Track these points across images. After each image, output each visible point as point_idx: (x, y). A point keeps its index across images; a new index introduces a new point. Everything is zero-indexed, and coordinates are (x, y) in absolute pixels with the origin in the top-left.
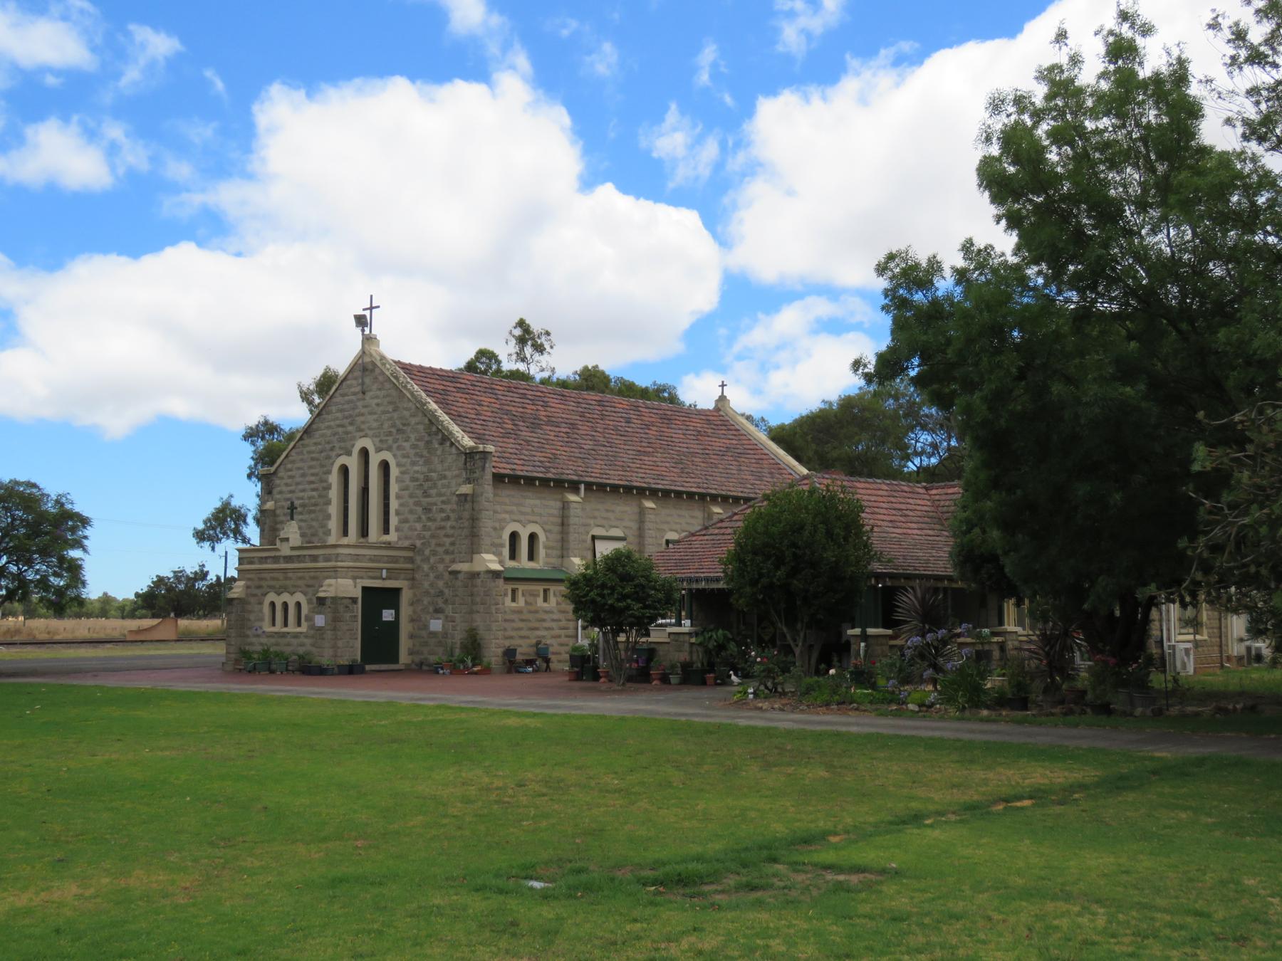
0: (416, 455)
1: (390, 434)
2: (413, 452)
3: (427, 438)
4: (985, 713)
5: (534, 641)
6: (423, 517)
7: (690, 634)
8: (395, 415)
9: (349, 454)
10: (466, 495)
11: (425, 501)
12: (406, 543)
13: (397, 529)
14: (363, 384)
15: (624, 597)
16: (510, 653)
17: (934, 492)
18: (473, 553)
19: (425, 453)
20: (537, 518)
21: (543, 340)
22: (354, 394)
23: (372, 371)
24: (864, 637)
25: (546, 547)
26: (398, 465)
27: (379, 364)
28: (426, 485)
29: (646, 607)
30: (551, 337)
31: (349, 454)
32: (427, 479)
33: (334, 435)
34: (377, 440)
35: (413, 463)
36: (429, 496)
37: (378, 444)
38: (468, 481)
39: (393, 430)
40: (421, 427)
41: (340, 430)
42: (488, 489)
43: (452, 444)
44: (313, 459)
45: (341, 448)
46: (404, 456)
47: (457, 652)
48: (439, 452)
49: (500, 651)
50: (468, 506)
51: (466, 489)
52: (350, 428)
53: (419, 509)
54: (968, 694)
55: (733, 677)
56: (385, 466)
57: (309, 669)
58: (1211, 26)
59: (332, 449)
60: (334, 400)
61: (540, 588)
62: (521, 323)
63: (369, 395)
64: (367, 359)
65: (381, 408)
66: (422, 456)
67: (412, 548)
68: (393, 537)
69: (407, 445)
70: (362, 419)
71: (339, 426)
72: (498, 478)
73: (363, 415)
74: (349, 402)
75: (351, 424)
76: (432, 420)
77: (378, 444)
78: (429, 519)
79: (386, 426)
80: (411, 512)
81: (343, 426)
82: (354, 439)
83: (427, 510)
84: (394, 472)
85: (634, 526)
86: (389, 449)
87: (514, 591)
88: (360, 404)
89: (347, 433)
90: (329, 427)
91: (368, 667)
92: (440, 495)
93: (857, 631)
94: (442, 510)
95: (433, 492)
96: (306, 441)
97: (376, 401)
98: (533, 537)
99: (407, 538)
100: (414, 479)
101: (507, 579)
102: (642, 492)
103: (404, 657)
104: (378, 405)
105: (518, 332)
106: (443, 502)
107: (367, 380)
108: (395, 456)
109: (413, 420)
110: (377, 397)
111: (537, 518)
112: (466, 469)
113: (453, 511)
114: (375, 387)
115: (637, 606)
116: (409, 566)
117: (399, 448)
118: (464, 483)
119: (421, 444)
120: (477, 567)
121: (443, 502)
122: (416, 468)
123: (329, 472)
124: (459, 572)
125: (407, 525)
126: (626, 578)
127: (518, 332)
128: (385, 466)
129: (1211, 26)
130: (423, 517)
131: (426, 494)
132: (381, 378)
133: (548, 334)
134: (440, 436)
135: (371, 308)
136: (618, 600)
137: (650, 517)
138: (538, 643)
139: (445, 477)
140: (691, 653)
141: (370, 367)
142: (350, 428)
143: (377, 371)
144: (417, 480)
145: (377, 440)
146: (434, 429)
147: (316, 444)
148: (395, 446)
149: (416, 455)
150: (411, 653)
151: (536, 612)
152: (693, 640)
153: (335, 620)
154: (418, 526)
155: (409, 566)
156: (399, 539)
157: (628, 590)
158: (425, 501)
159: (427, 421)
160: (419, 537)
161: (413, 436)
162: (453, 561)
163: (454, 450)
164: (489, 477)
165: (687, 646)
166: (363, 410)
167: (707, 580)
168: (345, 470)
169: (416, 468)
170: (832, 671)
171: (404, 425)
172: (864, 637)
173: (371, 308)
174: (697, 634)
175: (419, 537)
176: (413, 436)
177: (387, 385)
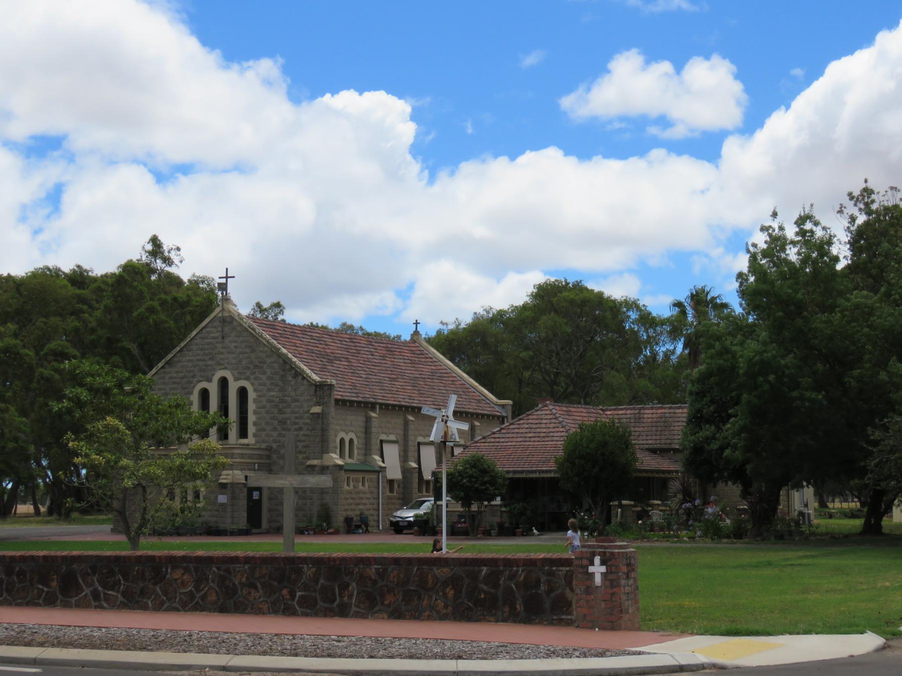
0: (272, 384)
1: (248, 368)
2: (268, 382)
3: (281, 373)
4: (725, 540)
5: (358, 513)
6: (278, 427)
7: (501, 506)
8: (253, 356)
9: (209, 380)
10: (318, 414)
11: (280, 417)
12: (264, 446)
13: (255, 435)
14: (223, 331)
15: (485, 483)
16: (348, 520)
17: (609, 413)
18: (323, 453)
19: (280, 383)
20: (353, 429)
21: (173, 255)
22: (214, 338)
23: (231, 323)
24: (620, 506)
25: (358, 448)
26: (255, 390)
27: (237, 318)
28: (281, 406)
29: (496, 489)
30: (182, 253)
31: (209, 380)
32: (282, 401)
33: (195, 366)
34: (236, 372)
35: (269, 390)
36: (285, 413)
37: (237, 375)
38: (318, 404)
39: (251, 366)
40: (276, 365)
41: (201, 363)
42: (332, 410)
43: (304, 378)
44: (174, 383)
45: (201, 376)
46: (260, 385)
47: (315, 519)
48: (293, 383)
49: (342, 519)
50: (320, 421)
51: (317, 409)
52: (210, 362)
53: (276, 423)
54: (714, 532)
55: (535, 531)
56: (243, 393)
57: (232, 533)
58: (838, 212)
59: (194, 376)
60: (195, 341)
61: (360, 476)
62: (155, 241)
63: (227, 340)
64: (226, 314)
65: (239, 350)
66: (277, 385)
67: (269, 449)
68: (250, 440)
69: (264, 377)
70: (222, 356)
71: (199, 360)
72: (337, 401)
73: (222, 353)
74: (208, 344)
75: (211, 359)
76: (286, 361)
77: (237, 375)
78: (284, 429)
79: (244, 362)
80: (267, 423)
81: (202, 360)
82: (214, 370)
83: (282, 422)
84: (252, 395)
85: (401, 432)
86: (247, 379)
87: (348, 478)
88: (219, 346)
89: (207, 366)
90: (189, 361)
91: (254, 531)
92: (293, 412)
93: (616, 503)
94: (296, 423)
95: (288, 410)
96: (168, 370)
97: (233, 344)
98: (351, 441)
99: (264, 442)
100: (269, 401)
101: (346, 470)
102: (372, 406)
103: (265, 525)
104: (236, 347)
105: (149, 247)
106: (297, 418)
107: (226, 329)
108: (252, 384)
109: (269, 360)
110: (235, 342)
111: (353, 429)
112: (316, 395)
113: (305, 424)
114: (234, 334)
115: (492, 489)
116: (267, 461)
117: (256, 379)
118: (315, 405)
119: (277, 377)
120: (327, 463)
121: (297, 418)
122: (272, 394)
123: (191, 393)
124: (315, 466)
125: (264, 433)
126: (484, 472)
127: (149, 247)
128: (243, 393)
129: (838, 212)
130: (278, 427)
131: (281, 411)
132: (239, 329)
133: (178, 249)
134: (293, 372)
135: (227, 277)
136: (481, 485)
137: (411, 427)
138: (361, 514)
139: (297, 401)
140: (501, 517)
141: (228, 319)
142: (210, 362)
143: (235, 323)
144: (273, 401)
145: (236, 372)
146: (288, 367)
147: (177, 372)
148: (252, 377)
149: (272, 384)
150: (269, 521)
151: (359, 493)
152: (504, 509)
153: (233, 498)
154: (275, 434)
155: (267, 461)
156: (257, 442)
157: (486, 479)
158: (280, 417)
159: (281, 361)
160: (275, 441)
161: (269, 372)
162: (308, 458)
163: (305, 382)
164: (333, 402)
165: (499, 513)
166: (222, 350)
167: (515, 472)
168: (205, 394)
169: (272, 394)
170: (640, 522)
171: (260, 363)
172: (620, 506)
173: (227, 277)
174: (505, 506)
175: (275, 441)
176: (269, 372)
177: (245, 334)
